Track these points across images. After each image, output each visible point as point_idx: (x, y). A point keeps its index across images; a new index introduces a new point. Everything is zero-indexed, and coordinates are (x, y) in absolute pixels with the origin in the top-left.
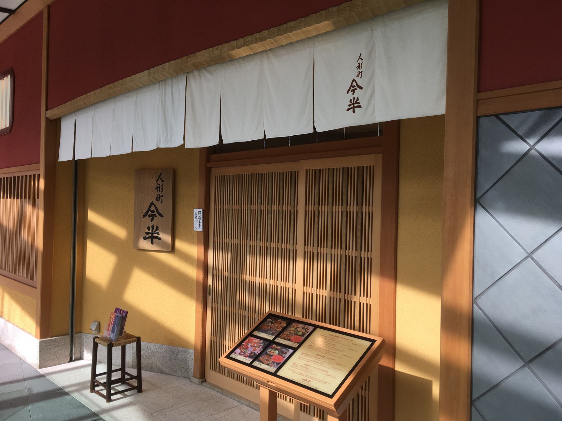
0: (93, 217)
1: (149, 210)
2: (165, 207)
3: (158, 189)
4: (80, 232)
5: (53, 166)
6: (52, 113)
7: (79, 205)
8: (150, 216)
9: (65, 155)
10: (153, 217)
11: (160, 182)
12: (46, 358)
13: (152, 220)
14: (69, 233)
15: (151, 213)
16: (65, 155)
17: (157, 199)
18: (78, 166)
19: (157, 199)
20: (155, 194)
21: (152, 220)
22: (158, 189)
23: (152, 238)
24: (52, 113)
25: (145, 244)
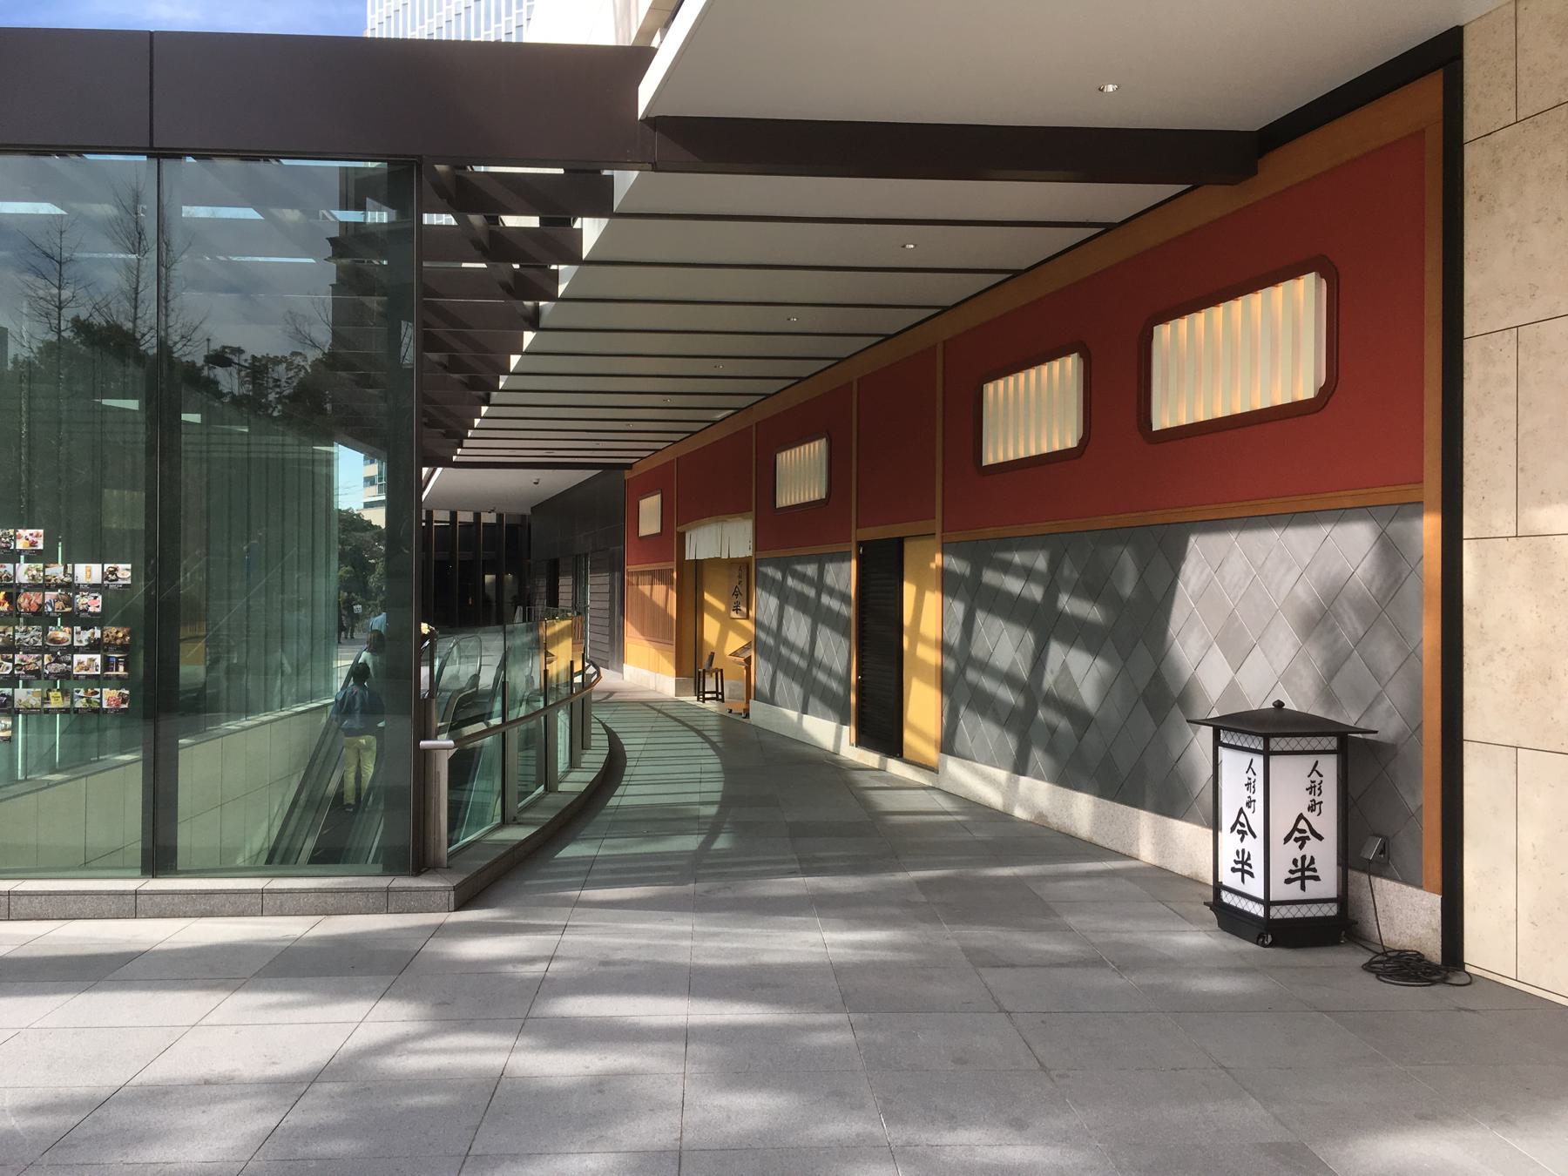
0: (707, 596)
1: (1295, 828)
2: (743, 589)
3: (1311, 789)
4: (699, 608)
5: (682, 563)
6: (680, 529)
7: (698, 591)
8: (1296, 840)
9: (689, 556)
10: (1302, 841)
11: (1315, 776)
12: (150, 236)
13: (1301, 847)
14: (691, 609)
15: (736, 593)
16: (689, 556)
17: (1311, 809)
18: (698, 563)
19: (1311, 809)
20: (1307, 799)
21: (1301, 847)
22: (1311, 789)
23: (737, 610)
24: (680, 529)
25: (734, 614)
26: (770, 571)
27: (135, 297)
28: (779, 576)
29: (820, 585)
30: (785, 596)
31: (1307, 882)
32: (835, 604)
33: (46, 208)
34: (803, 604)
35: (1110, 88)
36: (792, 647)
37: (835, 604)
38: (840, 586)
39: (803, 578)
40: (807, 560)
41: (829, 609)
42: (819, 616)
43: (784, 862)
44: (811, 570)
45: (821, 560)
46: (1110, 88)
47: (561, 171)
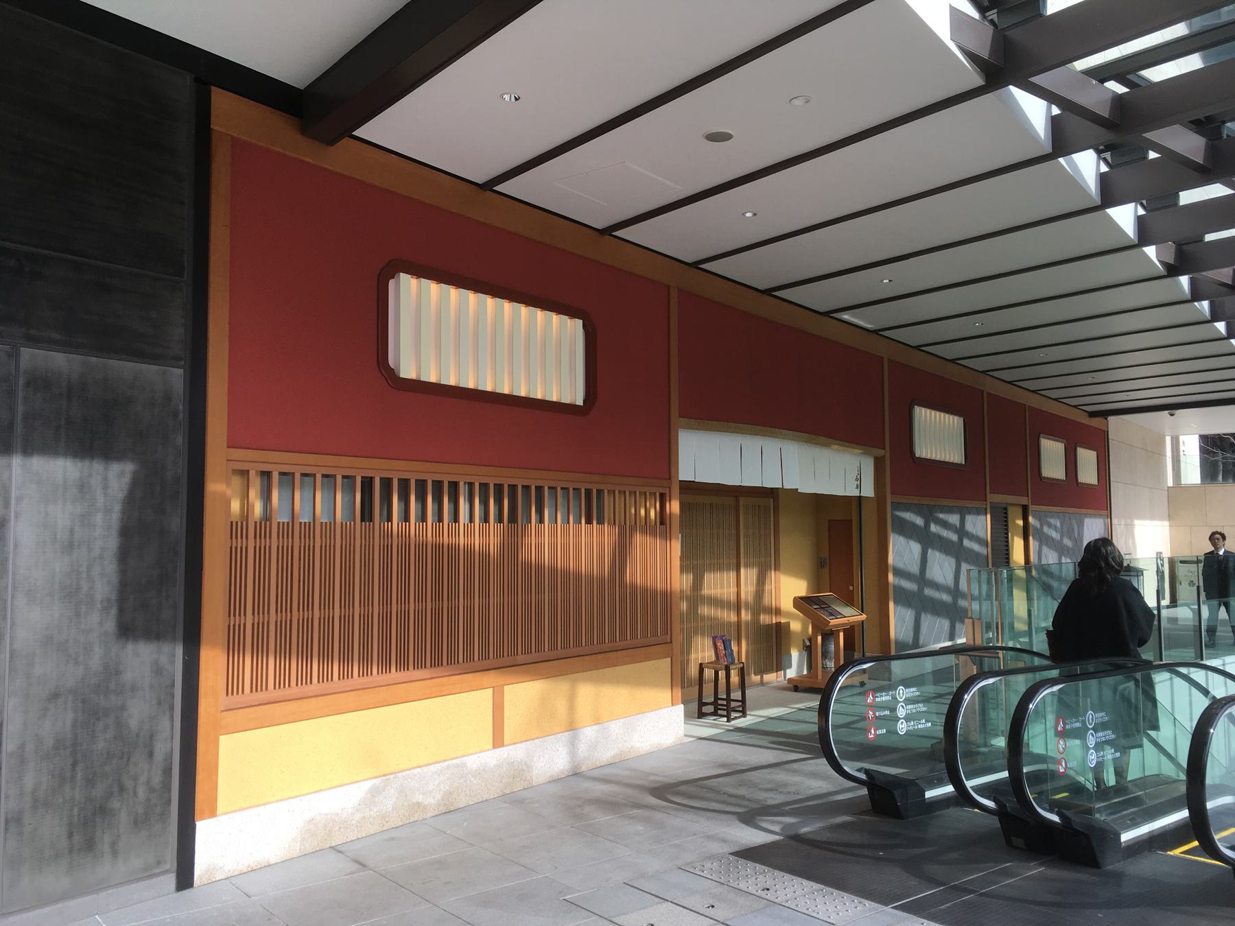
26: (908, 516)
27: (940, 696)
28: (919, 521)
29: (962, 532)
30: (928, 541)
31: (915, 569)
32: (976, 547)
33: (901, 771)
34: (945, 547)
35: (748, 215)
36: (936, 586)
37: (976, 547)
38: (981, 534)
39: (945, 524)
40: (950, 510)
41: (971, 551)
42: (957, 552)
43: (469, 610)
44: (954, 519)
45: (963, 513)
46: (748, 215)
47: (1210, 237)
